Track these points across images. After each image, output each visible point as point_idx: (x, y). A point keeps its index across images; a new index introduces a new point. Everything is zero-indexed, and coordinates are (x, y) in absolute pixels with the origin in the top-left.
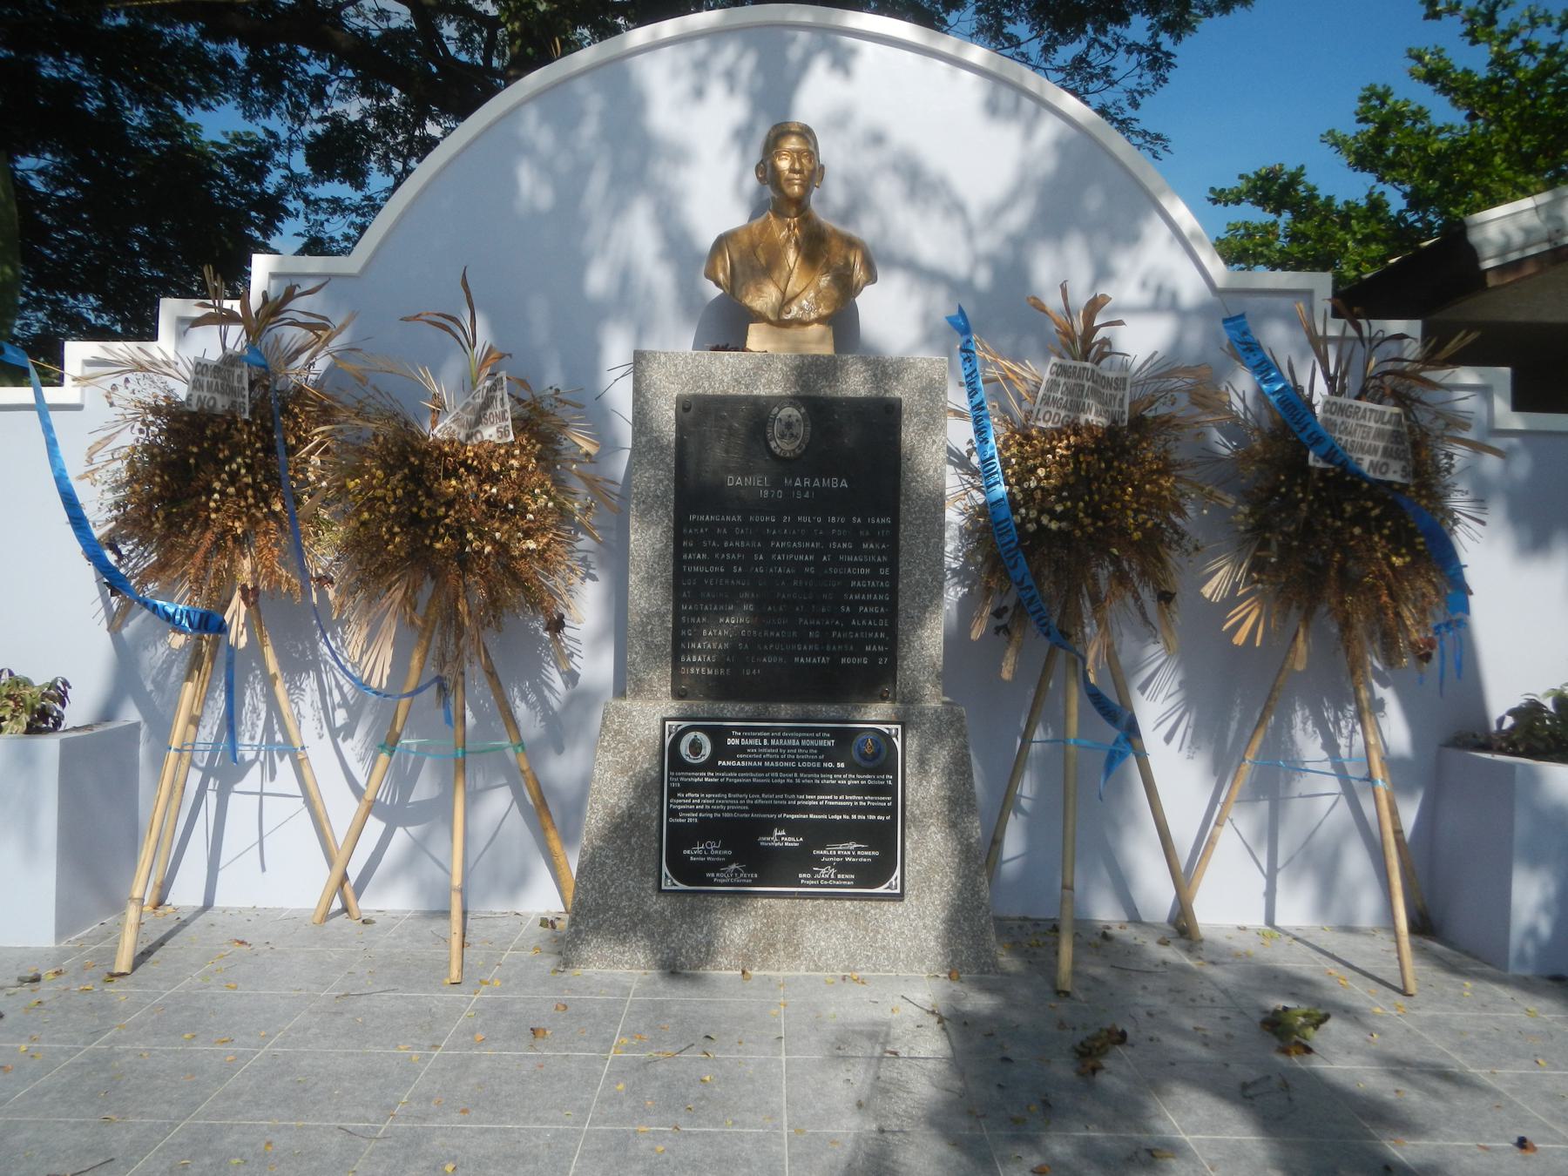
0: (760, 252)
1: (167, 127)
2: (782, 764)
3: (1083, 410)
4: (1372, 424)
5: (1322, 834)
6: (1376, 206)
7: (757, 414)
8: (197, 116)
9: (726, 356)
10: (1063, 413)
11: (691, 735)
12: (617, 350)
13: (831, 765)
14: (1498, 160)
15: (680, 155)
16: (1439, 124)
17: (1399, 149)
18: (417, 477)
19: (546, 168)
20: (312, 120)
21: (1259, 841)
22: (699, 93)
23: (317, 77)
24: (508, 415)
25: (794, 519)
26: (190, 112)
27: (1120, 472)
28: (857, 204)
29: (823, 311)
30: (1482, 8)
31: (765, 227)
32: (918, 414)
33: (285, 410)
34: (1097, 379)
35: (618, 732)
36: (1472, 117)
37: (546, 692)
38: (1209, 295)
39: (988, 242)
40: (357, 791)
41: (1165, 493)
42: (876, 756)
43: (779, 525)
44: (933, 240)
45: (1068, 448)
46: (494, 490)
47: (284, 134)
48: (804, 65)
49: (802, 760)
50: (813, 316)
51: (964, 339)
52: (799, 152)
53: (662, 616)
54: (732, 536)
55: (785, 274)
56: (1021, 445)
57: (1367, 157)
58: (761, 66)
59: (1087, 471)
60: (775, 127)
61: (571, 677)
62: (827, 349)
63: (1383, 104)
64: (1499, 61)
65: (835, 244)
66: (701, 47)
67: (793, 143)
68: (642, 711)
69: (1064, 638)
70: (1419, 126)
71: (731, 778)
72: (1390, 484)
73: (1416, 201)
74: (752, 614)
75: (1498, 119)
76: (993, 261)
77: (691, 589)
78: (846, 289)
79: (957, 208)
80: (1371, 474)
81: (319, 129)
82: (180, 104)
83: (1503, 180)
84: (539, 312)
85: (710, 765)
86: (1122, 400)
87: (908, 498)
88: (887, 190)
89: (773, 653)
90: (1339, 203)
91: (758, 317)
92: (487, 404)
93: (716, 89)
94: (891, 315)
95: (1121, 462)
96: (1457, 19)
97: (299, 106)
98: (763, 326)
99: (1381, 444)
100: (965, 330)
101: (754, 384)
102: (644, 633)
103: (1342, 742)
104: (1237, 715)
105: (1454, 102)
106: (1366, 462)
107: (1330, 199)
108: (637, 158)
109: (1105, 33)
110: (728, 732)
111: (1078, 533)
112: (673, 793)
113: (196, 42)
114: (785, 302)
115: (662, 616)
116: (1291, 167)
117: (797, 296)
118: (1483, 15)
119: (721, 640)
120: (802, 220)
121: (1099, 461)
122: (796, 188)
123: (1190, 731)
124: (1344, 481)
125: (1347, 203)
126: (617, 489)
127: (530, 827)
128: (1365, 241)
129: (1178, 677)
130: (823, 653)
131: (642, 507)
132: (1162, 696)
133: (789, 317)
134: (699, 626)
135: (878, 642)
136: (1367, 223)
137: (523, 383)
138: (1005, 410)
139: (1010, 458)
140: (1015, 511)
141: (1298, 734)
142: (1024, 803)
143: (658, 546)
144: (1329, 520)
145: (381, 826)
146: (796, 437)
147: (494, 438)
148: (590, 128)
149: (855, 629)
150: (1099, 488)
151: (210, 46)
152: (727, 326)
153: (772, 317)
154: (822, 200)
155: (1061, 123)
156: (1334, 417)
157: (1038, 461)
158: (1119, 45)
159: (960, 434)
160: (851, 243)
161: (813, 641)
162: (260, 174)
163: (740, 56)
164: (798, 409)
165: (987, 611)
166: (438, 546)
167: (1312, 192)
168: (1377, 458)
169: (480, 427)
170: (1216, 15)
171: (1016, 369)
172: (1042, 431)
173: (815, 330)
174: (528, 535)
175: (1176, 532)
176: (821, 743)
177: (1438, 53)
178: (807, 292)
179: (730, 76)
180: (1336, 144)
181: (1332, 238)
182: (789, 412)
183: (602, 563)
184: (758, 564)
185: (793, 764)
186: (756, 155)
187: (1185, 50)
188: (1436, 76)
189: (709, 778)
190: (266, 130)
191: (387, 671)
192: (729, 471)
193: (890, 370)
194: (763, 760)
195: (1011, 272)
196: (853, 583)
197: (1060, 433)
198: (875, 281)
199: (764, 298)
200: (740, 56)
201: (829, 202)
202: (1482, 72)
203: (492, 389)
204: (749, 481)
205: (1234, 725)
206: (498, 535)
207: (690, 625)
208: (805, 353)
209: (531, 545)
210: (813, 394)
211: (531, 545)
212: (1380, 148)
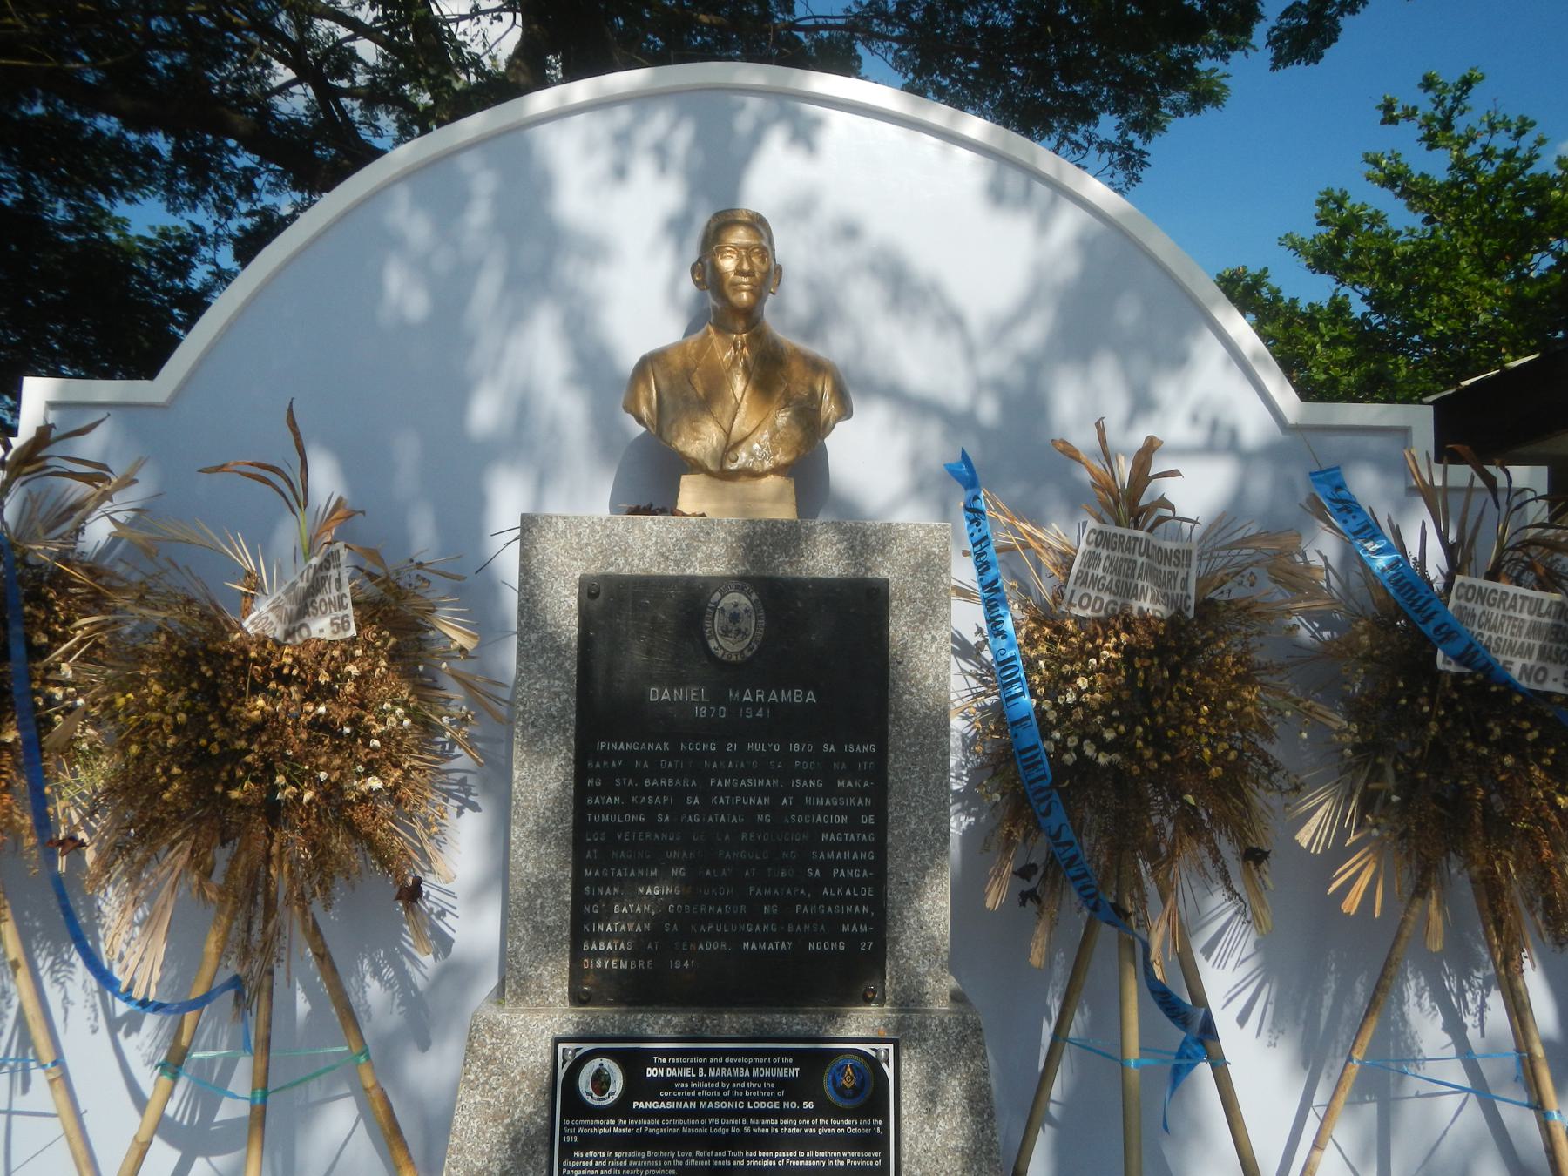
0: (696, 379)
1: (90, 220)
2: (724, 1105)
3: (1135, 596)
4: (1525, 616)
5: (1446, 1147)
6: (1339, 308)
7: (688, 602)
8: (121, 209)
9: (648, 521)
10: (1106, 598)
11: (595, 1064)
12: (508, 501)
13: (794, 1105)
14: (1463, 263)
15: (596, 250)
16: (1395, 228)
17: (1357, 251)
18: (210, 690)
19: (421, 266)
20: (240, 214)
21: (1364, 1157)
22: (620, 173)
23: (245, 169)
24: (348, 601)
25: (742, 747)
26: (113, 205)
27: (1191, 682)
28: (824, 315)
29: (781, 458)
30: (1438, 114)
31: (704, 344)
32: (912, 601)
33: (37, 598)
34: (1152, 551)
35: (490, 1060)
36: (1429, 221)
37: (408, 965)
38: (1278, 433)
39: (993, 364)
40: (140, 1101)
41: (1249, 709)
42: (857, 1091)
43: (721, 755)
44: (923, 361)
45: (1116, 648)
46: (322, 709)
47: (210, 229)
48: (756, 139)
49: (752, 1099)
50: (768, 465)
51: (970, 493)
52: (748, 248)
53: (556, 886)
54: (656, 773)
55: (729, 409)
56: (1051, 641)
57: (1325, 259)
58: (700, 139)
59: (1145, 681)
60: (717, 215)
61: (443, 943)
62: (785, 512)
63: (1340, 207)
64: (1460, 164)
65: (796, 367)
66: (623, 115)
67: (740, 237)
68: (526, 1026)
69: (1114, 912)
70: (1376, 229)
71: (650, 1126)
72: (1548, 696)
73: (1379, 302)
74: (683, 882)
75: (1459, 223)
76: (998, 387)
77: (601, 837)
78: (811, 428)
79: (953, 320)
80: (1524, 683)
81: (248, 223)
82: (101, 196)
83: (1468, 283)
84: (407, 450)
85: (621, 1108)
86: (1185, 580)
87: (899, 716)
88: (863, 297)
89: (712, 936)
90: (1303, 305)
91: (694, 467)
92: (316, 587)
93: (643, 169)
94: (869, 458)
95: (1190, 670)
96: (1413, 125)
97: (226, 199)
98: (701, 478)
99: (1537, 643)
100: (971, 482)
101: (687, 560)
102: (531, 910)
103: (1469, 1020)
104: (1331, 985)
105: (1411, 206)
106: (1516, 667)
107: (1294, 301)
108: (540, 253)
109: (1075, 131)
110: (647, 1057)
111: (1136, 770)
112: (567, 1152)
113: (119, 133)
114: (730, 446)
115: (556, 886)
116: (1254, 270)
117: (746, 438)
118: (1439, 121)
119: (638, 918)
120: (753, 337)
121: (1161, 665)
122: (745, 296)
123: (1270, 1008)
124: (1485, 690)
125: (1311, 305)
126: (505, 694)
127: (383, 1160)
128: (1333, 343)
129: (1253, 937)
130: (783, 936)
131: (531, 731)
132: (1232, 962)
133: (734, 466)
134: (609, 901)
135: (859, 919)
136: (1334, 325)
137: (373, 554)
138: (1025, 589)
139: (1036, 660)
140: (1045, 735)
141: (1412, 1011)
142: (1053, 1109)
143: (553, 786)
144: (1470, 745)
145: (174, 1156)
146: (745, 635)
147: (328, 635)
148: (479, 215)
149: (829, 901)
150: (1164, 705)
151: (132, 136)
152: (652, 481)
153: (711, 466)
154: (779, 309)
155: (1083, 215)
156: (1470, 605)
157: (1078, 667)
158: (1090, 142)
159: (968, 618)
160: (817, 366)
161: (768, 919)
162: (184, 270)
163: (674, 126)
164: (748, 595)
165: (1008, 870)
166: (235, 794)
167: (1276, 294)
168: (1530, 662)
169: (306, 620)
170: (1186, 114)
171: (1039, 534)
172: (1079, 620)
173: (771, 483)
174: (371, 769)
175: (1266, 763)
176: (782, 1072)
177: (1395, 158)
178: (759, 432)
179: (661, 151)
180: (1295, 248)
181: (1300, 341)
182: (737, 600)
183: (486, 786)
184: (693, 810)
185: (740, 1105)
186: (692, 254)
187: (1158, 148)
188: (1394, 179)
189: (620, 1127)
190: (192, 224)
191: (157, 975)
192: (653, 681)
193: (873, 541)
194: (697, 1099)
195: (1026, 403)
196: (824, 836)
197: (1104, 625)
198: (850, 417)
199: (702, 441)
200: (674, 126)
201: (786, 315)
202: (1441, 176)
203: (325, 565)
204: (679, 694)
205: (1328, 1001)
206: (323, 775)
207: (597, 899)
208: (757, 517)
209: (375, 783)
210: (767, 573)
211: (375, 783)
212: (1338, 251)
